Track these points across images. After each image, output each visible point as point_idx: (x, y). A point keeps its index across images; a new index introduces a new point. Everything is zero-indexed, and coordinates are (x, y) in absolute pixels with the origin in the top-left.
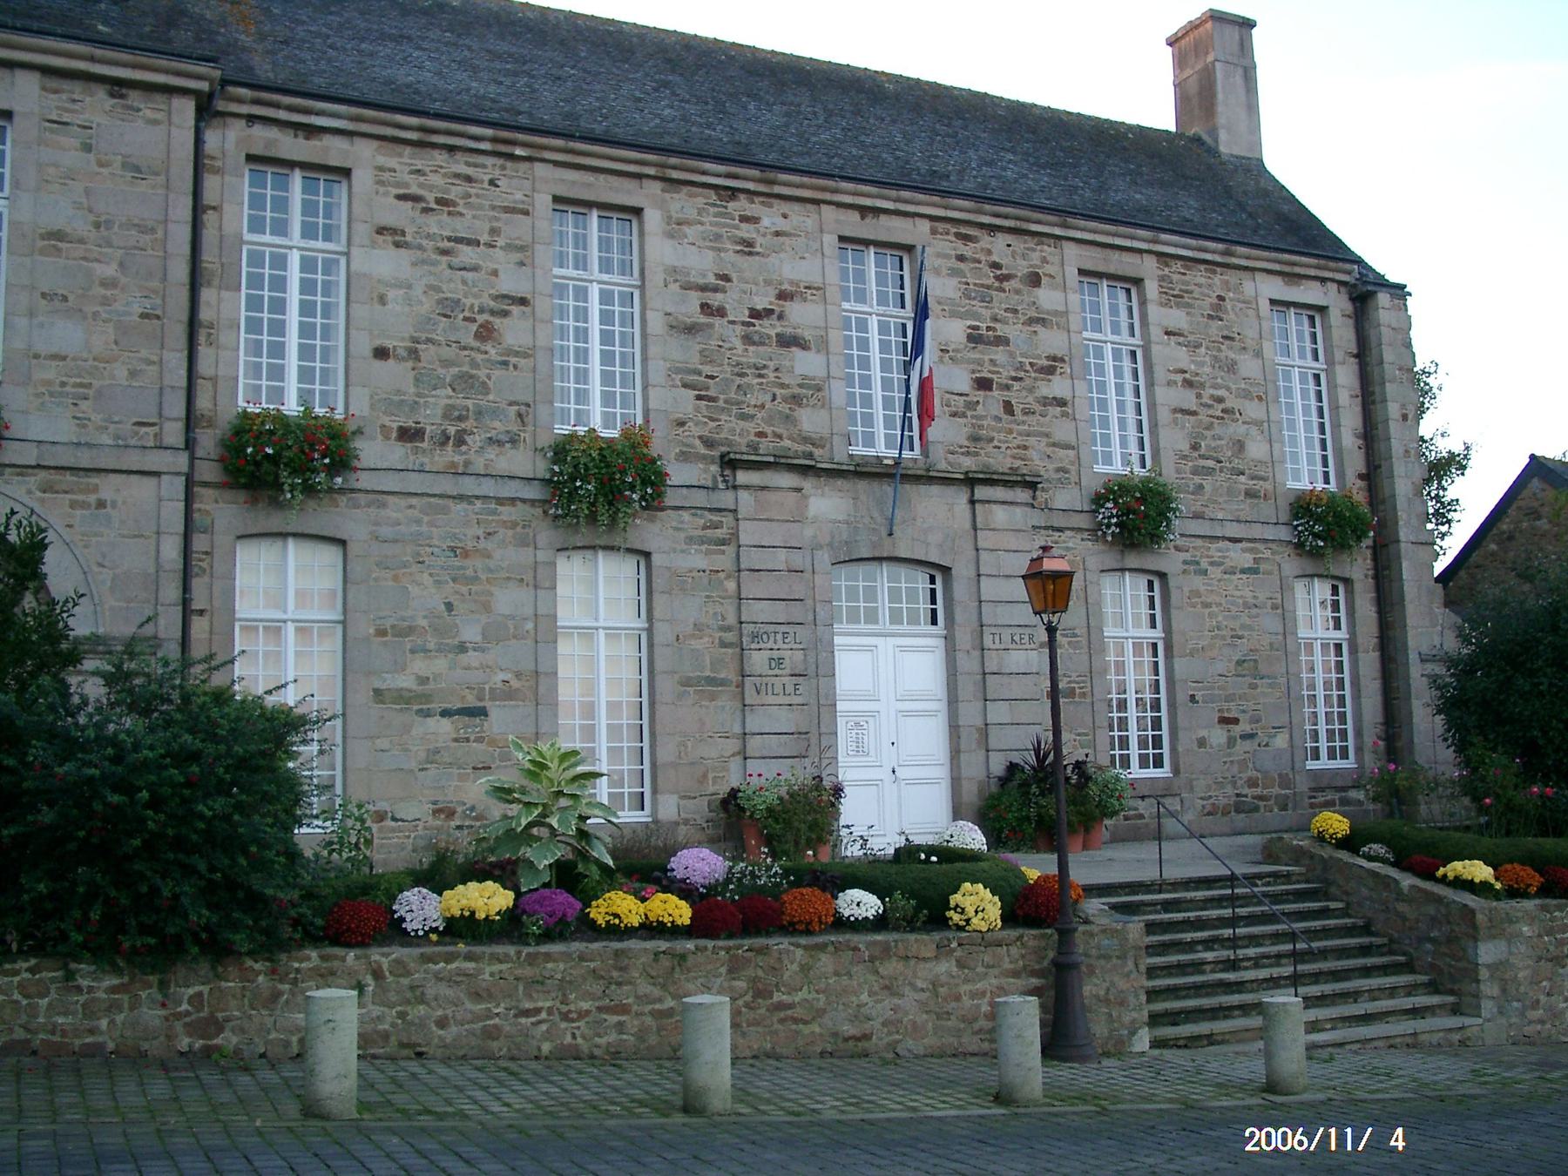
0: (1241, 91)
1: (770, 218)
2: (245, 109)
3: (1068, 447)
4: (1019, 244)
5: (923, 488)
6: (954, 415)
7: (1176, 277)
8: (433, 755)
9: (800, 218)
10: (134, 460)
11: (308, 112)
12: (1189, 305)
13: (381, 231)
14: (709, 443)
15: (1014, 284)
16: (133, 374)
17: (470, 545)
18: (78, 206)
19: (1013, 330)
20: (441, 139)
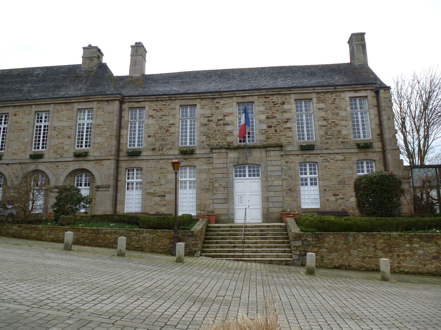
0: (361, 50)
1: (222, 102)
2: (128, 101)
3: (291, 137)
4: (279, 97)
5: (254, 150)
6: (262, 134)
7: (321, 97)
8: (156, 204)
9: (228, 100)
10: (107, 158)
11: (138, 99)
12: (325, 102)
13: (150, 116)
14: (208, 145)
15: (278, 105)
16: (108, 144)
17: (163, 167)
18: (102, 120)
19: (278, 115)
20: (159, 99)
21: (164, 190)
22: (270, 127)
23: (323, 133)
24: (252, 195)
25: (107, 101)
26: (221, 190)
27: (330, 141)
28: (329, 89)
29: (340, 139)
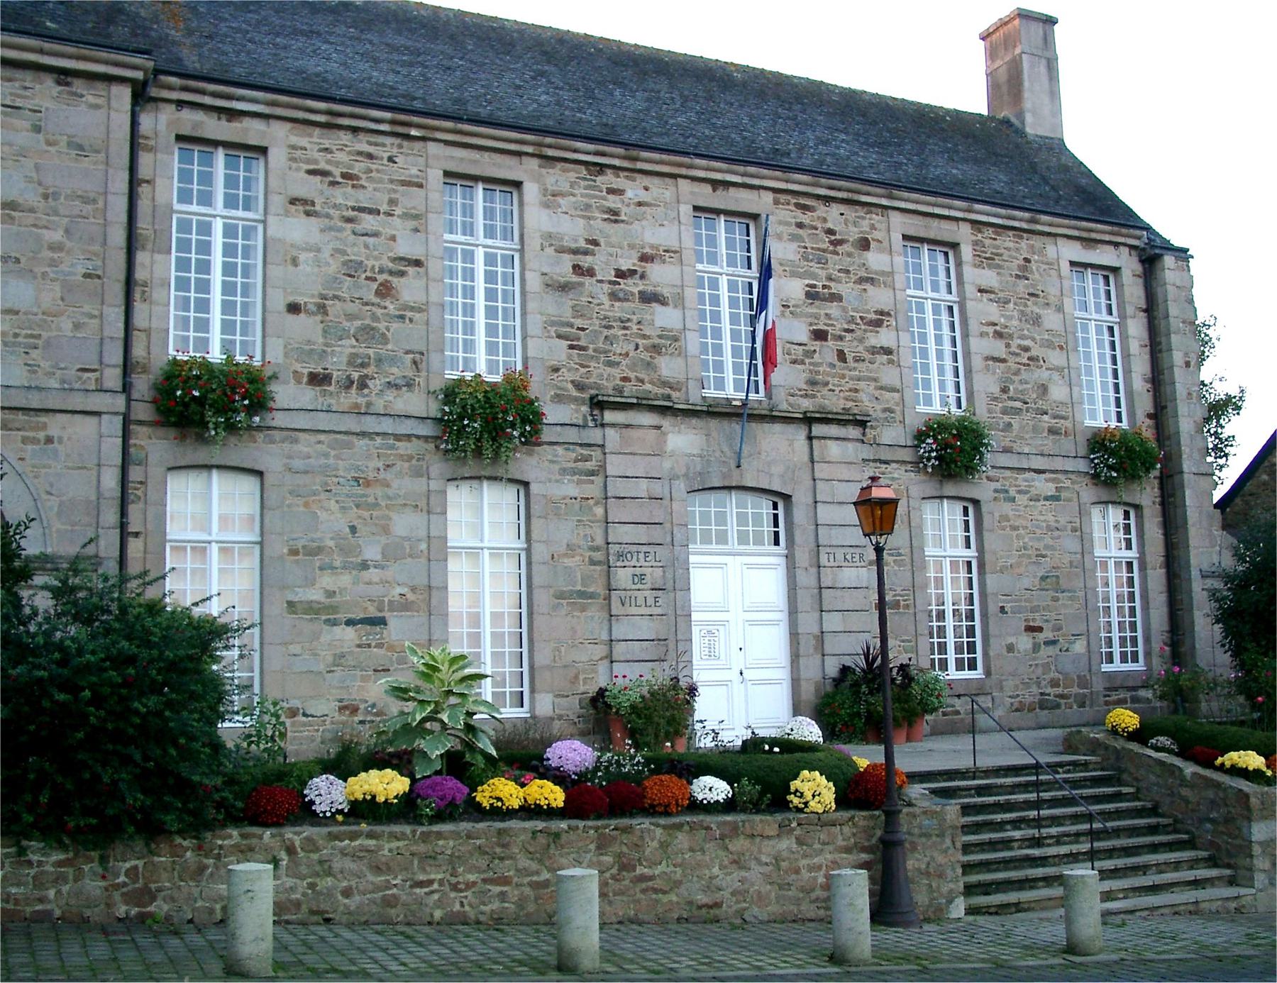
1: (634, 190)
2: (175, 95)
3: (894, 390)
5: (766, 426)
6: (794, 362)
7: (987, 242)
8: (339, 660)
10: (78, 402)
12: (999, 267)
13: (293, 201)
14: (580, 387)
15: (846, 248)
16: (77, 326)
17: (371, 475)
18: (29, 180)
21: (376, 591)
22: (820, 335)
23: (996, 390)
24: (753, 623)
25: (64, 76)
26: (640, 601)
27: (1016, 422)
28: (1014, 219)
29: (1046, 417)
